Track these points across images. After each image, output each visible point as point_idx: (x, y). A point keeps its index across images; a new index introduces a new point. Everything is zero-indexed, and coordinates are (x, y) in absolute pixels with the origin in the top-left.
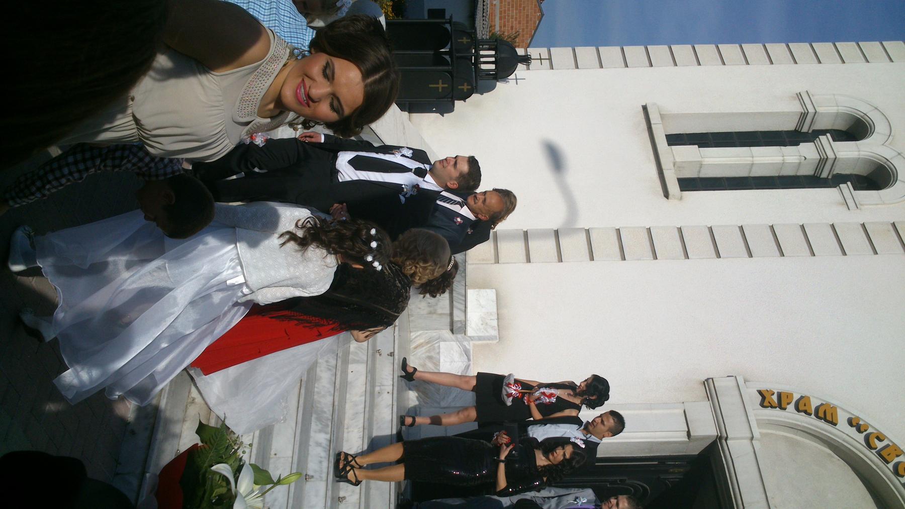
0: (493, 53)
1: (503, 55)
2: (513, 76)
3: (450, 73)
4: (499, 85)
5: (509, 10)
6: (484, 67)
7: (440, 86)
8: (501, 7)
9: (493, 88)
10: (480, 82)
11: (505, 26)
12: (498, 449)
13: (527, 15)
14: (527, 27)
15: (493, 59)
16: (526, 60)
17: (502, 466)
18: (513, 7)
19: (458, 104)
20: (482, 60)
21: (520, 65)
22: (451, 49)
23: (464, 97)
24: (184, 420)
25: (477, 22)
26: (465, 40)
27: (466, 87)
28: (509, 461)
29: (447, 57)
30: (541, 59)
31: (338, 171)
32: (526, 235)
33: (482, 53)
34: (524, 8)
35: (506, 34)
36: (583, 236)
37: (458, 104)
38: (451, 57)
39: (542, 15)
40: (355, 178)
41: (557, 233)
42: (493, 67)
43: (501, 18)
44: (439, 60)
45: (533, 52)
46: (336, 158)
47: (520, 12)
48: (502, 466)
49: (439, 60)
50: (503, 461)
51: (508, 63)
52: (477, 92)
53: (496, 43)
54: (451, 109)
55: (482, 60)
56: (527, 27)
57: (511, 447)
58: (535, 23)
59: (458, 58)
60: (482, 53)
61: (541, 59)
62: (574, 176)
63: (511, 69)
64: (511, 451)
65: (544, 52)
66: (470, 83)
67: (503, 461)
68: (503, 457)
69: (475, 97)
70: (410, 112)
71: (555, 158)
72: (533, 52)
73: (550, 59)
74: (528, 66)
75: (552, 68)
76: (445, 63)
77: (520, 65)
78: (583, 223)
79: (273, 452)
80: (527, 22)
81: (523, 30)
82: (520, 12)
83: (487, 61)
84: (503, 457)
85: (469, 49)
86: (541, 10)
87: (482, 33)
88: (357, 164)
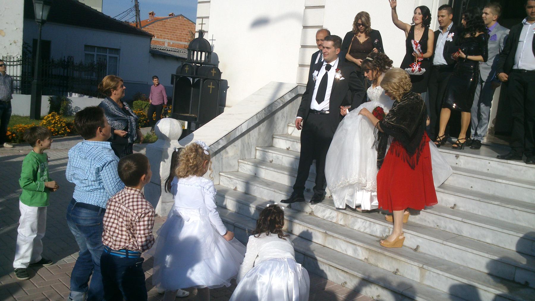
0: (195, 52)
1: (198, 47)
2: (210, 42)
3: (204, 80)
4: (215, 51)
5: (177, 35)
6: (203, 59)
7: (211, 87)
8: (175, 40)
9: (216, 55)
10: (212, 62)
11: (185, 39)
12: (461, 58)
13: (181, 24)
14: (187, 25)
15: (199, 53)
16: (201, 33)
17: (469, 57)
18: (175, 33)
19: (223, 77)
20: (199, 59)
21: (205, 37)
22: (191, 77)
23: (219, 73)
24: (377, 266)
25: (180, 56)
26: (187, 69)
27: (213, 72)
28: (467, 53)
29: (196, 80)
30: (202, 24)
31: (322, 110)
32: (303, 47)
33: (195, 59)
34: (176, 26)
35: (190, 39)
36: (308, 10)
37: (223, 77)
38: (196, 78)
39: (181, 15)
40: (329, 101)
41: (305, 27)
42: (204, 53)
43: (181, 41)
44: (196, 85)
45: (198, 28)
46: (314, 111)
47: (178, 29)
48: (469, 57)
49: (196, 85)
50: (467, 57)
51: (201, 44)
52: (218, 65)
53: (191, 49)
54: (225, 82)
55: (199, 59)
56: (187, 25)
57: (460, 51)
58: (185, 20)
59: (196, 74)
60: (195, 59)
61: (202, 24)
62: (272, 13)
63: (206, 43)
64: (462, 51)
65: (198, 21)
66: (212, 69)
67: (467, 57)
68: (464, 56)
69: (220, 67)
70: (225, 106)
71: (260, 22)
72: (198, 28)
73: (202, 18)
74: (205, 32)
75: (208, 17)
76: (198, 81)
77: (205, 37)
78: (301, 9)
79: (470, 189)
80: (185, 25)
81: (189, 28)
82: (178, 29)
83: (200, 56)
84: (464, 56)
85: (191, 66)
86: (178, 16)
87: (184, 55)
88: (320, 99)
